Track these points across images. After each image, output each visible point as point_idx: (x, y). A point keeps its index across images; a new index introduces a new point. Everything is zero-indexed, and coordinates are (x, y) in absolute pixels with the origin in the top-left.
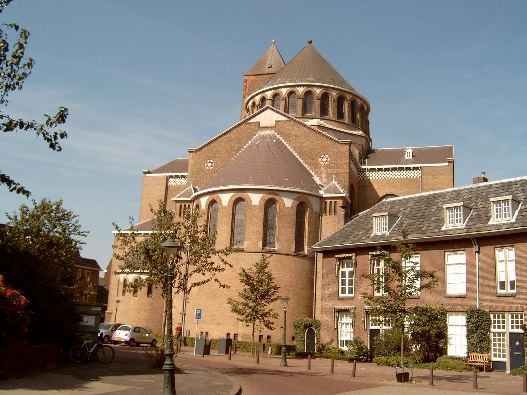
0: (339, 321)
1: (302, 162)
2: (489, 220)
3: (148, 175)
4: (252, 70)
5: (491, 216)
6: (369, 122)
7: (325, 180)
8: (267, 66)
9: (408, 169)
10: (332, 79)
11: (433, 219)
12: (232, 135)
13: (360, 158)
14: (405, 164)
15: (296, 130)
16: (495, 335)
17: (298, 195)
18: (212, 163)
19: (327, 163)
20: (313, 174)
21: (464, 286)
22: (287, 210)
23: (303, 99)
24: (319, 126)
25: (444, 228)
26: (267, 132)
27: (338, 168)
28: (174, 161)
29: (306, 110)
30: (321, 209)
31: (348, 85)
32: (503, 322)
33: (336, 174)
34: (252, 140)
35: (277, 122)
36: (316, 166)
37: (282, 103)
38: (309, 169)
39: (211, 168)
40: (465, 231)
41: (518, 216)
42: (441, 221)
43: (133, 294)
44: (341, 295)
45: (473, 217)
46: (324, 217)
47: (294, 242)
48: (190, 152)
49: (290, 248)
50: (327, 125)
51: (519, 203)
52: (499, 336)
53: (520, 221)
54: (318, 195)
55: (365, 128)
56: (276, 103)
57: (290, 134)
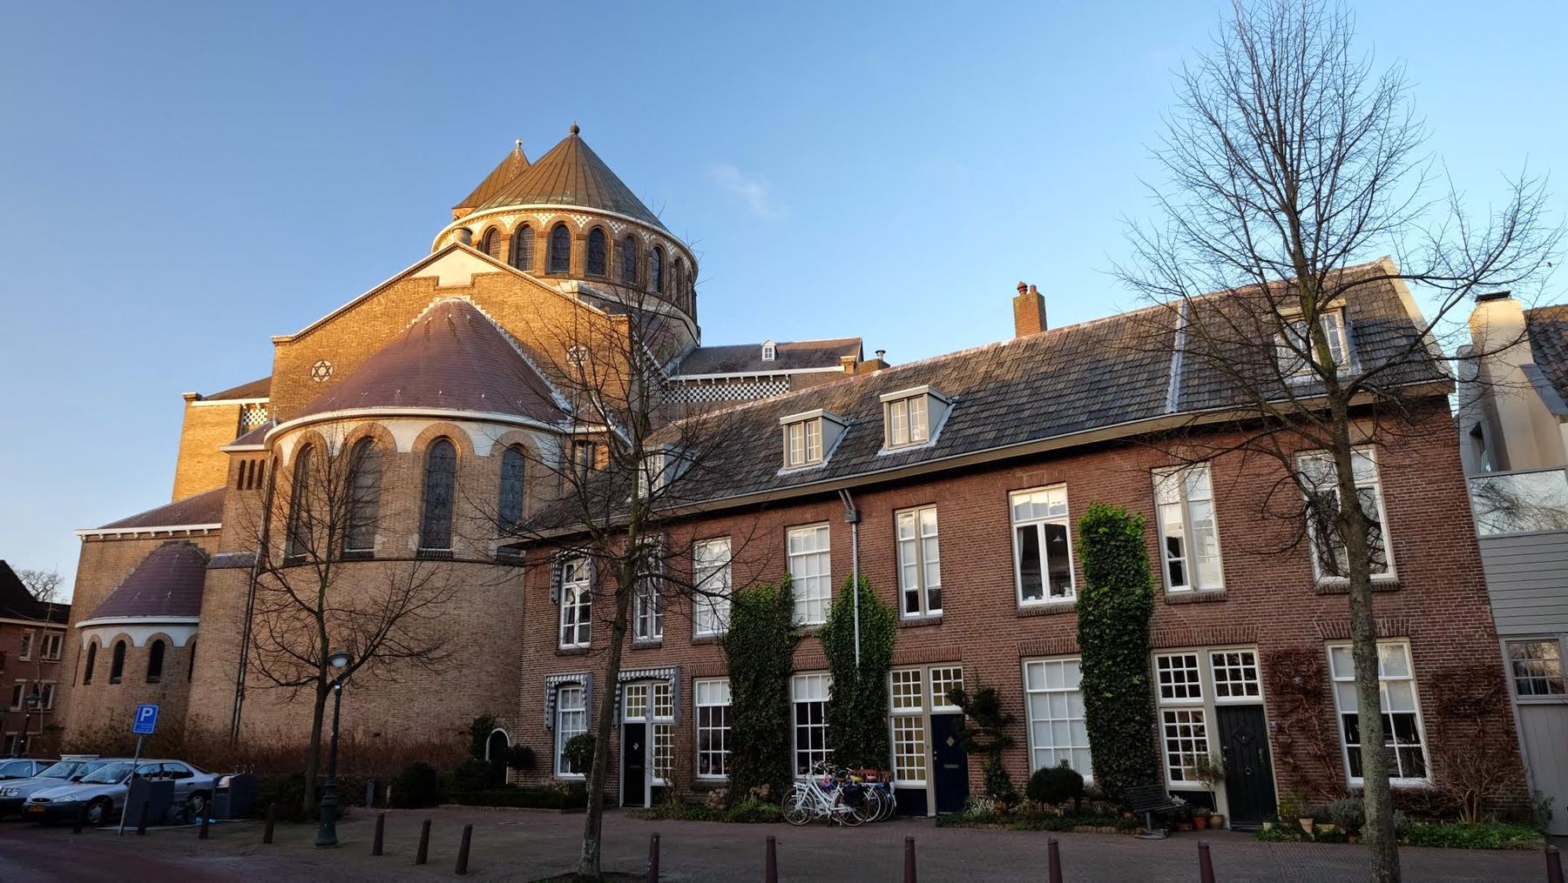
0: (560, 709)
2: (880, 446)
3: (195, 403)
5: (884, 439)
9: (762, 378)
12: (376, 306)
14: (757, 370)
16: (898, 725)
22: (480, 462)
23: (548, 237)
25: (780, 473)
34: (420, 316)
35: (475, 277)
37: (504, 247)
39: (326, 378)
40: (826, 473)
43: (111, 678)
44: (564, 646)
45: (848, 442)
48: (277, 343)
52: (909, 724)
53: (948, 443)
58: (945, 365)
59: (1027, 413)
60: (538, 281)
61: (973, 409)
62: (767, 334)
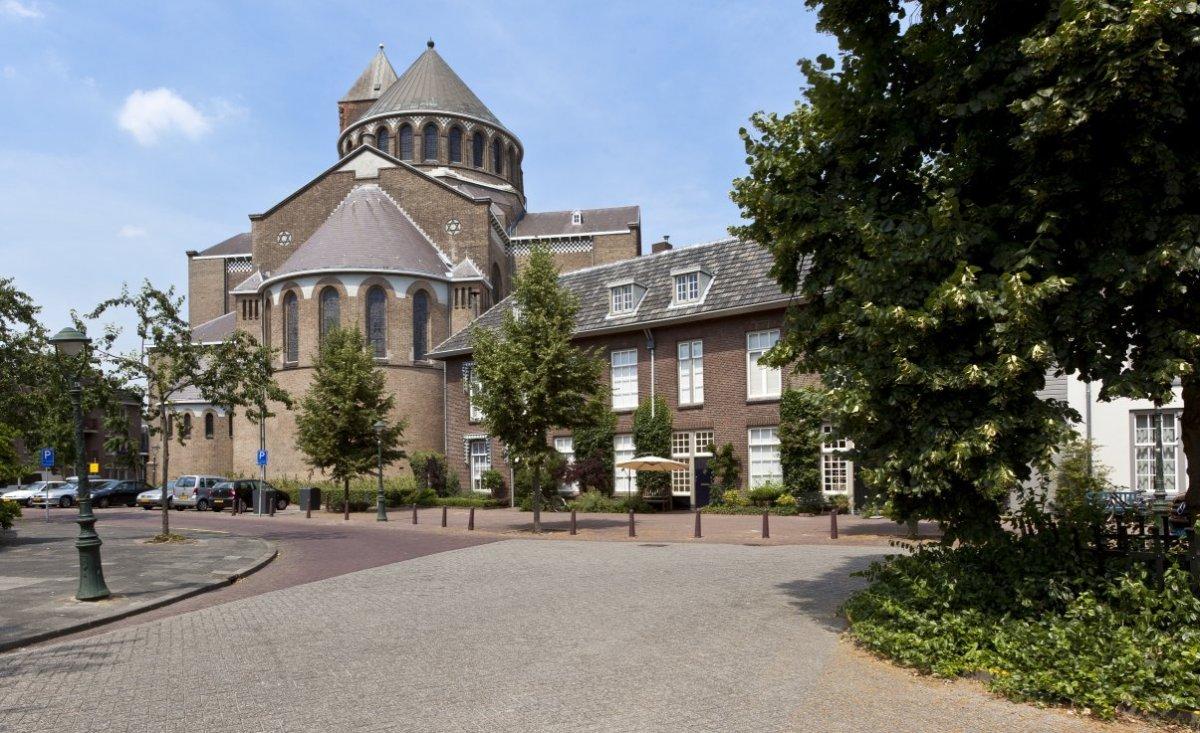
1: (421, 231)
2: (669, 302)
3: (194, 258)
4: (351, 94)
6: (521, 173)
7: (454, 258)
8: (373, 87)
9: (575, 239)
10: (464, 104)
11: (595, 304)
12: (316, 191)
13: (508, 226)
15: (410, 183)
16: (827, 458)
17: (412, 281)
18: (288, 236)
19: (456, 232)
20: (438, 248)
21: (635, 398)
24: (447, 178)
26: (368, 187)
27: (473, 239)
28: (240, 235)
29: (428, 152)
30: (450, 300)
31: (490, 114)
32: (687, 443)
33: (471, 248)
36: (441, 237)
38: (431, 241)
41: (708, 295)
42: (605, 308)
46: (454, 312)
47: (412, 348)
49: (407, 357)
50: (459, 177)
51: (711, 277)
54: (445, 278)
55: (517, 179)
56: (383, 144)
57: (401, 189)
58: (709, 249)
59: (760, 284)
60: (417, 169)
61: (727, 281)
62: (576, 205)
